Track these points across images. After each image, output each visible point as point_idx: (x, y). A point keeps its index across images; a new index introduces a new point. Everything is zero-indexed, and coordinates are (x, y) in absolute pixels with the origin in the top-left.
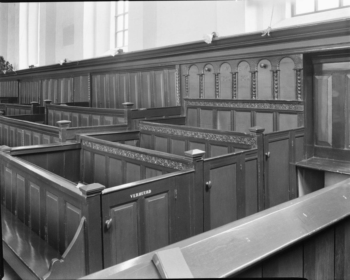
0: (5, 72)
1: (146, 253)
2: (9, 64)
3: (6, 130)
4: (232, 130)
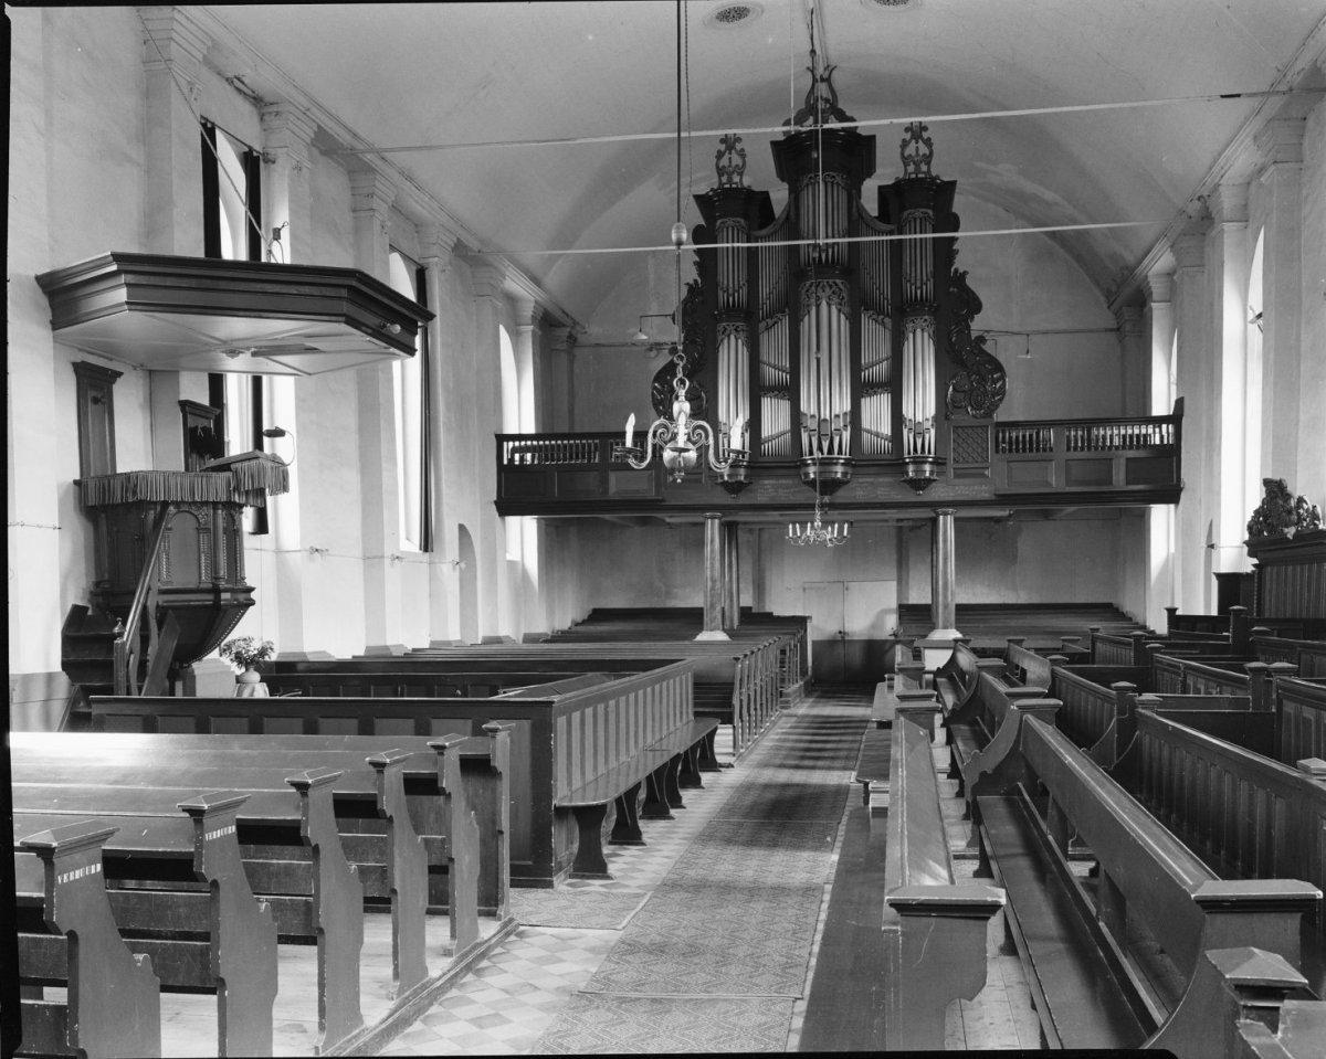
0: (1291, 532)
1: (300, 487)
2: (1305, 505)
3: (1307, 722)
4: (918, 230)
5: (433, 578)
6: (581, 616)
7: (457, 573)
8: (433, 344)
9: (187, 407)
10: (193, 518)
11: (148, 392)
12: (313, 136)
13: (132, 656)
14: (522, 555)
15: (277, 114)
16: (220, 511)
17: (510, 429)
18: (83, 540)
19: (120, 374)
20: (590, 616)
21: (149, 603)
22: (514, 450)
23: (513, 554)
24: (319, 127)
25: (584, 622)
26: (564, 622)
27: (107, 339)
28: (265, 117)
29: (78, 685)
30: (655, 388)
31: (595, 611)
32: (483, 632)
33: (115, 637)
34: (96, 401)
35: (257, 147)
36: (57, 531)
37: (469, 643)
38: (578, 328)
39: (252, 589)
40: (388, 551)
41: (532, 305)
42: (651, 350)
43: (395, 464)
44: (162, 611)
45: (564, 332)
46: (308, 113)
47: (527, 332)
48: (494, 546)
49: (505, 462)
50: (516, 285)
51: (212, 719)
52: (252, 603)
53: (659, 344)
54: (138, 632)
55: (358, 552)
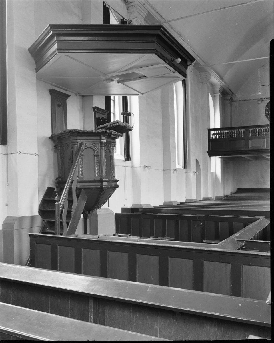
5: (187, 178)
6: (234, 190)
7: (195, 176)
8: (187, 96)
9: (95, 109)
10: (92, 151)
11: (82, 104)
12: (146, 15)
13: (64, 209)
14: (215, 171)
15: (133, 6)
16: (103, 148)
17: (212, 127)
18: (53, 161)
19: (69, 96)
20: (237, 191)
21: (72, 187)
22: (214, 135)
23: (213, 170)
24: (148, 12)
25: (235, 193)
26: (228, 192)
27: (62, 77)
28: (129, 8)
29: (46, 220)
30: (266, 109)
31: (239, 189)
32: (203, 196)
33: (55, 201)
34: (59, 106)
35: (126, 18)
36: (37, 156)
37: (199, 200)
38: (234, 95)
39: (118, 181)
40: (172, 168)
41: (220, 86)
42: (259, 101)
43: (175, 137)
44: (79, 192)
45: (229, 97)
46: (144, 6)
47: (217, 96)
48: (207, 166)
49: (211, 138)
50: (215, 79)
51: (83, 249)
52: (117, 187)
53: (262, 99)
54: (67, 198)
55: (161, 168)
